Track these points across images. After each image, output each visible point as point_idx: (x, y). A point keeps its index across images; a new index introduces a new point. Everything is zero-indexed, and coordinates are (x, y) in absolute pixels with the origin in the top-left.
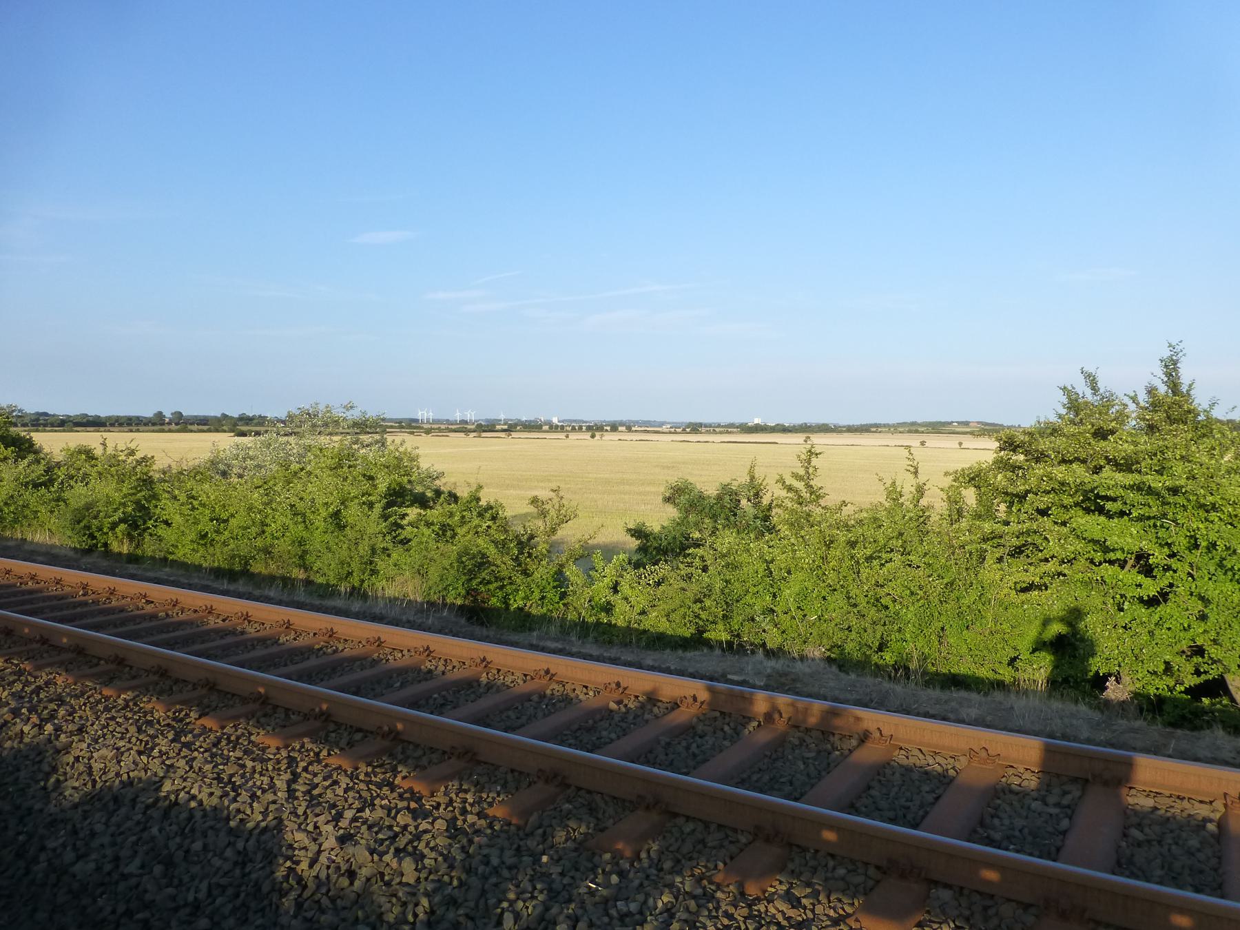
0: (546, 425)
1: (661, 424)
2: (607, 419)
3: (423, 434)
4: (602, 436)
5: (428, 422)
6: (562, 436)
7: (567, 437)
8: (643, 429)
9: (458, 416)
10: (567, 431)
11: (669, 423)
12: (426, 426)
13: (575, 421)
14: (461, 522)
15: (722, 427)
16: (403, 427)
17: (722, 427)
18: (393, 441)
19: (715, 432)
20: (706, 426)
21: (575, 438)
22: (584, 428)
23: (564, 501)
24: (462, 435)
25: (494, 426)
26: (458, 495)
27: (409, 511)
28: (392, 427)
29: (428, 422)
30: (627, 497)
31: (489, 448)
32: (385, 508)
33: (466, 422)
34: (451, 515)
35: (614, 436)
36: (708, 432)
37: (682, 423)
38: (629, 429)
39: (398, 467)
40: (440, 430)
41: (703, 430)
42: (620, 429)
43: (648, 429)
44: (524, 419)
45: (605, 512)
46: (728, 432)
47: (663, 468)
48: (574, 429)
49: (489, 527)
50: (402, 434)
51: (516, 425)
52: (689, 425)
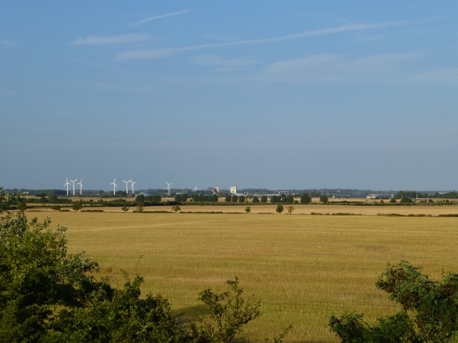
0: (222, 196)
1: (365, 194)
2: (297, 189)
3: (71, 210)
4: (291, 209)
5: (77, 194)
6: (242, 209)
7: (248, 210)
8: (341, 200)
9: (115, 187)
10: (248, 204)
11: (374, 193)
12: (74, 199)
13: (257, 191)
14: (116, 323)
15: (441, 196)
16: (46, 201)
17: (441, 196)
18: (35, 221)
19: (432, 203)
20: (420, 196)
21: (258, 211)
22: (269, 199)
23: (242, 296)
24: (119, 209)
25: (159, 198)
26: (112, 287)
27: (51, 308)
28: (32, 201)
29: (77, 194)
30: (323, 285)
31: (152, 226)
32: (21, 305)
33: (124, 194)
34: (104, 313)
35: (307, 210)
36: (423, 204)
37: (391, 192)
38: (324, 201)
39: (38, 254)
40: (92, 204)
41: (418, 200)
42: (314, 200)
43: (348, 200)
44: (195, 189)
45: (296, 305)
46: (448, 204)
47: (368, 248)
48: (256, 201)
49: (150, 329)
50: (45, 209)
51: (185, 197)
52: (400, 194)
